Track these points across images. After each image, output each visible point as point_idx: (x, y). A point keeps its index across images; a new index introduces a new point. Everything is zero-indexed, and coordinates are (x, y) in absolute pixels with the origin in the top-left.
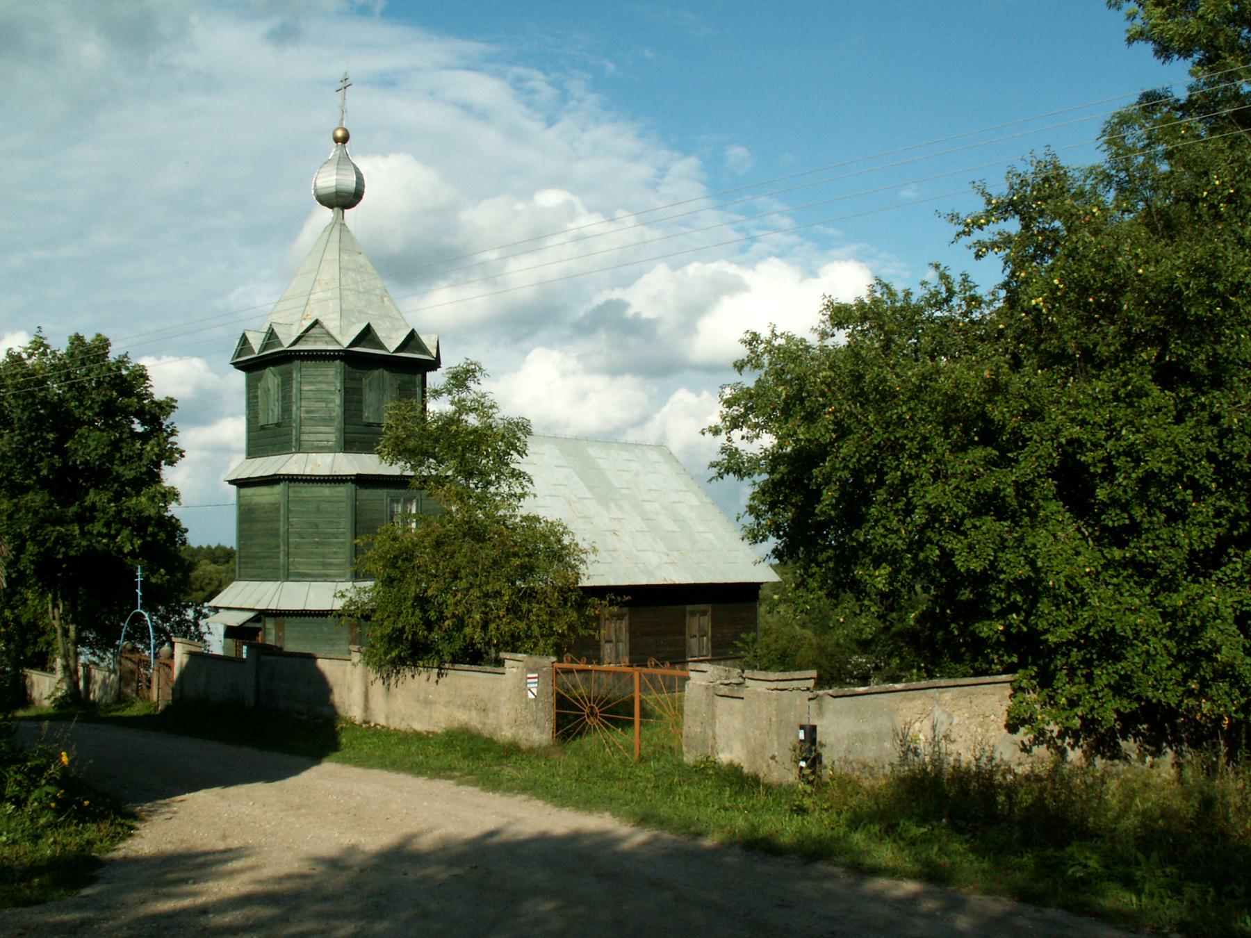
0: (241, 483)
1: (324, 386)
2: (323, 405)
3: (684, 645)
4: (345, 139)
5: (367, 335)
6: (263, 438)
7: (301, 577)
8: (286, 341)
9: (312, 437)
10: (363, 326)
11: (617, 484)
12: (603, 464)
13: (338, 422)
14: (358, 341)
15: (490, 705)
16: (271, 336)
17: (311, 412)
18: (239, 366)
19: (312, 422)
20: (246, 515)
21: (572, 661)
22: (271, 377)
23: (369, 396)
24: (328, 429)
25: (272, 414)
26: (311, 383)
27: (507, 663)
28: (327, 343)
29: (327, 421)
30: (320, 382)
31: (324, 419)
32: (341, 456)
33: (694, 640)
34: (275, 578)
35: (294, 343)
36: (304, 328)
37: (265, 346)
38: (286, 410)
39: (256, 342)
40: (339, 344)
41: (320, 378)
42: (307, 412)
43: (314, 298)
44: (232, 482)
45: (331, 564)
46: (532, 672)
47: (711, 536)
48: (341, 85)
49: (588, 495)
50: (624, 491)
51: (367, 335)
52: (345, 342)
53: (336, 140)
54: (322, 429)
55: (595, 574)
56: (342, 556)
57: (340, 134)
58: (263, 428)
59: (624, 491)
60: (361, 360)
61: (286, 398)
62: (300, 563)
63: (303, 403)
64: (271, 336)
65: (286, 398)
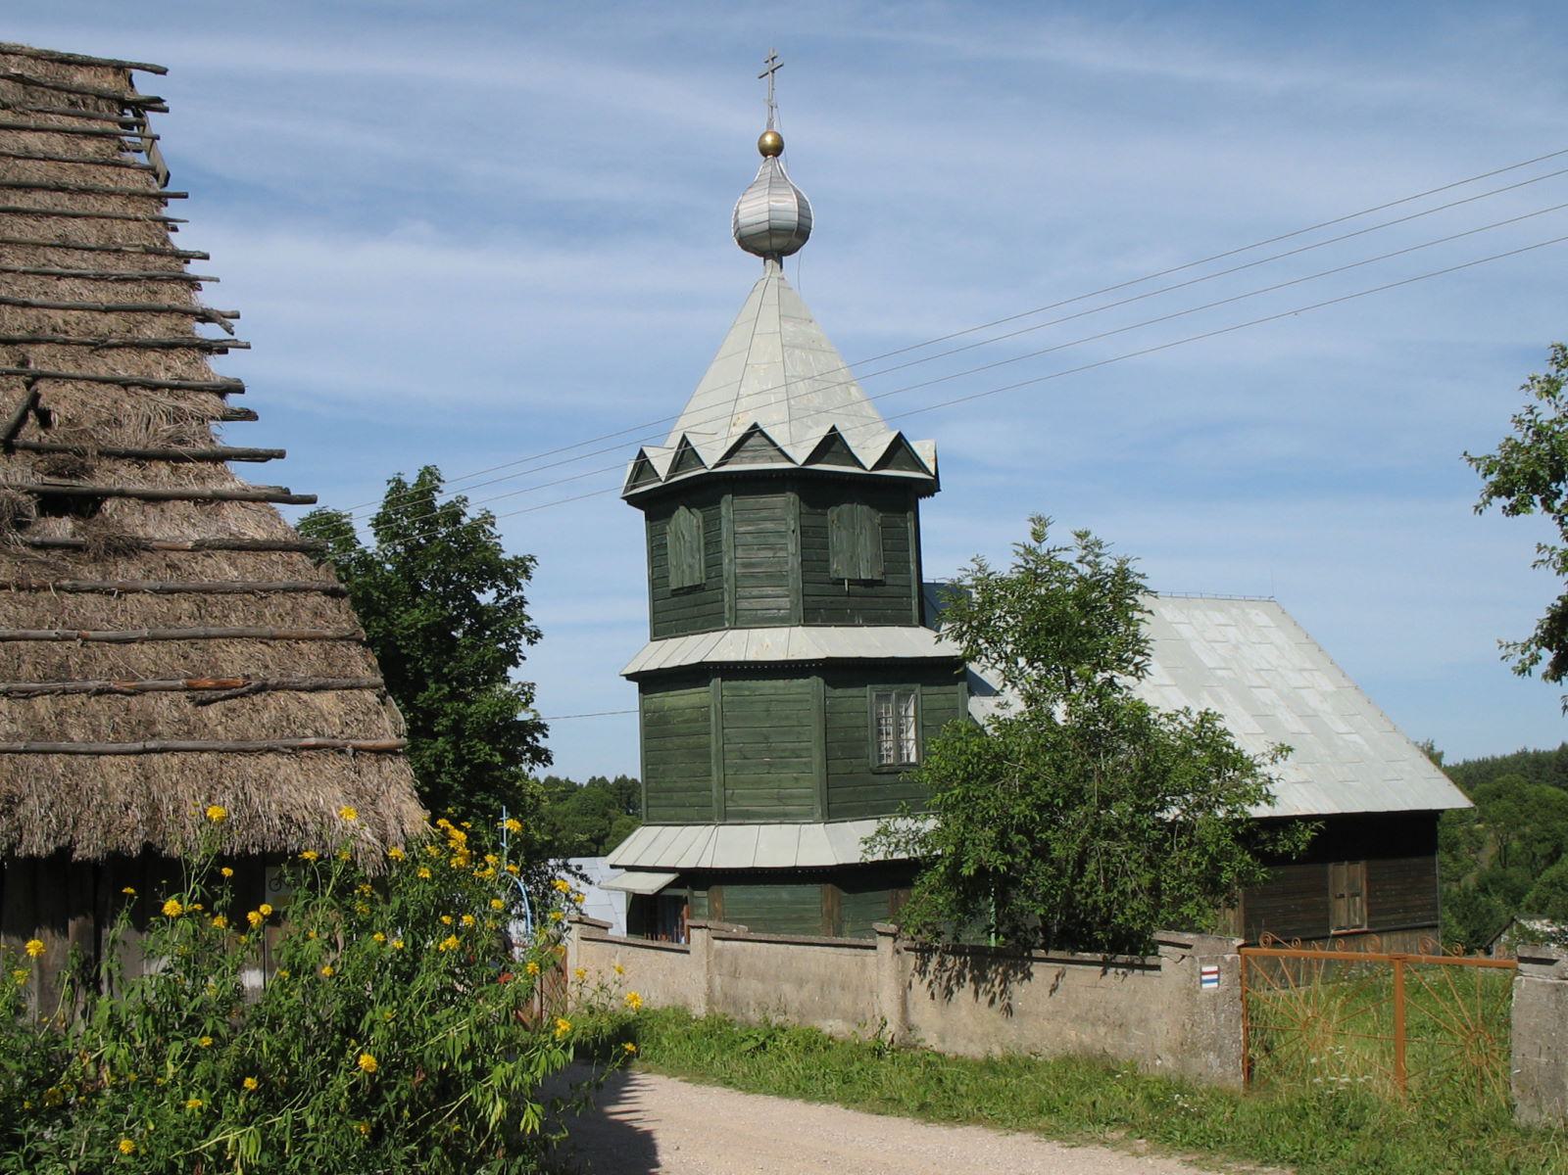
0: (650, 682)
1: (770, 525)
2: (770, 554)
3: (1327, 909)
4: (776, 150)
5: (832, 444)
6: (677, 606)
7: (745, 817)
8: (711, 454)
9: (755, 604)
10: (824, 431)
11: (1210, 662)
12: (1186, 631)
13: (795, 580)
14: (817, 455)
15: (1132, 1017)
16: (686, 454)
17: (752, 565)
18: (633, 501)
19: (752, 582)
20: (655, 730)
21: (1275, 943)
22: (686, 521)
23: (838, 537)
24: (779, 591)
25: (687, 569)
26: (750, 522)
27: (1162, 949)
28: (772, 459)
29: (776, 578)
30: (765, 519)
31: (770, 576)
32: (800, 632)
33: (1342, 903)
34: (706, 821)
35: (717, 465)
36: (735, 439)
37: (677, 465)
38: (713, 564)
39: (662, 462)
40: (790, 460)
41: (764, 514)
42: (745, 565)
43: (764, 384)
44: (630, 677)
45: (791, 796)
46: (1210, 963)
47: (1356, 738)
48: (766, 68)
49: (1168, 681)
50: (1220, 673)
51: (832, 444)
52: (800, 455)
53: (765, 151)
54: (769, 591)
55: (1299, 792)
56: (808, 783)
57: (769, 139)
58: (676, 593)
59: (1220, 673)
60: (825, 486)
61: (712, 543)
62: (742, 797)
63: (740, 553)
64: (686, 454)
65: (712, 543)
